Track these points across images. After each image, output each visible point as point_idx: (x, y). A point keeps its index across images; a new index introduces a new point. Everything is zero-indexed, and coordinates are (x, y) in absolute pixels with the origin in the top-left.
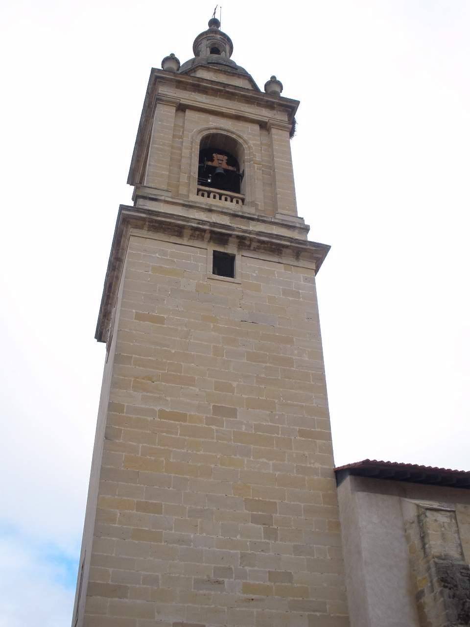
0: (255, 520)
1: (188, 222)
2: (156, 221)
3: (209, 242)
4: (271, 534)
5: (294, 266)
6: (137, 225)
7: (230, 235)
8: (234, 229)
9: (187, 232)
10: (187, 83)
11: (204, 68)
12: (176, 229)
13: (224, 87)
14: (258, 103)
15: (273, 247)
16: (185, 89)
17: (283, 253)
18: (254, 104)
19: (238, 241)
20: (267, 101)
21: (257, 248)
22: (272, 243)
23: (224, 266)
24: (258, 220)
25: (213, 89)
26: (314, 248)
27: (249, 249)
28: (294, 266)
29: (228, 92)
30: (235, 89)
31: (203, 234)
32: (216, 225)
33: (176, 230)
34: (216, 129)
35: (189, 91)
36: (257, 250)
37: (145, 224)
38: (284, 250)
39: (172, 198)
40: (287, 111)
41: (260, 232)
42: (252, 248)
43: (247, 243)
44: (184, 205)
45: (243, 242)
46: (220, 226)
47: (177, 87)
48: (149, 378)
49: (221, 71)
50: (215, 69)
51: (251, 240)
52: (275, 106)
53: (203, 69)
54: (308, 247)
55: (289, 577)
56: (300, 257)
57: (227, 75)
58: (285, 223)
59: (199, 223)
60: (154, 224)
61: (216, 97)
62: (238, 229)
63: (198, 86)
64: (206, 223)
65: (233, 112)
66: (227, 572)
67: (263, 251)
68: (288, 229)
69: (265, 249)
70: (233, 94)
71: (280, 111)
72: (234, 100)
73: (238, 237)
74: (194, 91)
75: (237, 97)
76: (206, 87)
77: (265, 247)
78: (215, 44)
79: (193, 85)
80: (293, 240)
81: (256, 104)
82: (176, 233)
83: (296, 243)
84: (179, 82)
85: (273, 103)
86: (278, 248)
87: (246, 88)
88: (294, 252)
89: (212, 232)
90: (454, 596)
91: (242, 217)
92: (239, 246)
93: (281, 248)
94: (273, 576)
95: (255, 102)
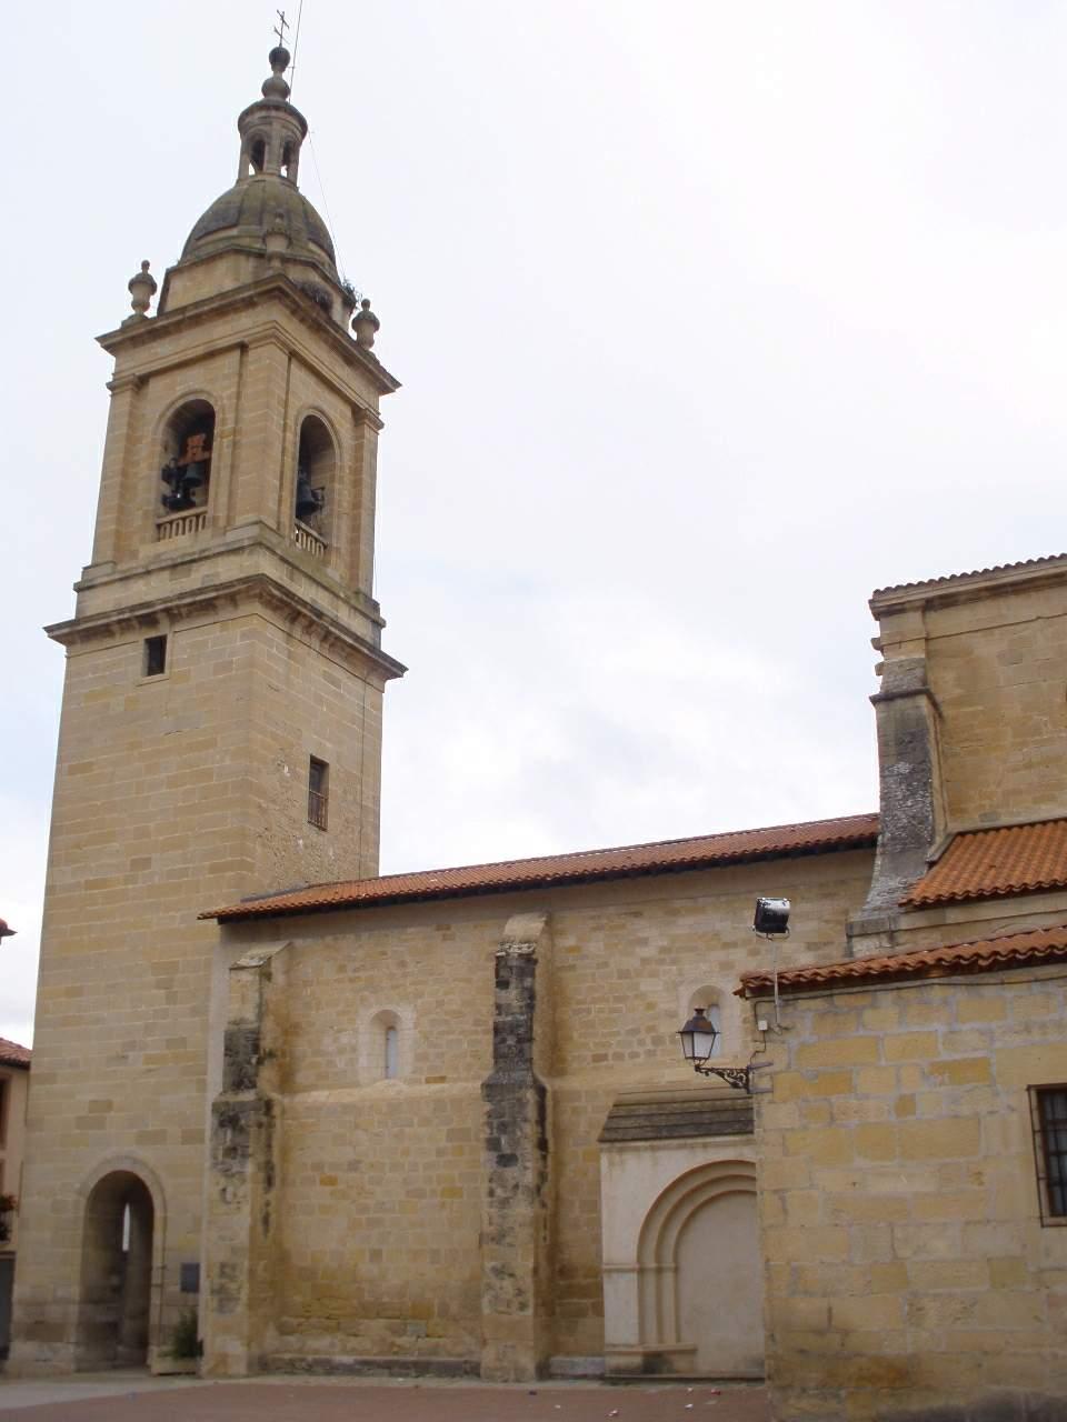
0: (159, 986)
3: (141, 628)
4: (171, 998)
10: (141, 335)
12: (103, 629)
16: (144, 343)
20: (243, 300)
23: (156, 656)
24: (200, 559)
29: (190, 318)
39: (108, 575)
40: (275, 297)
43: (176, 612)
44: (121, 579)
45: (173, 614)
48: (78, 846)
51: (178, 607)
55: (183, 1041)
63: (156, 330)
65: (200, 351)
66: (132, 1045)
69: (197, 610)
78: (253, 137)
83: (224, 588)
90: (232, 1064)
91: (183, 564)
94: (170, 1043)
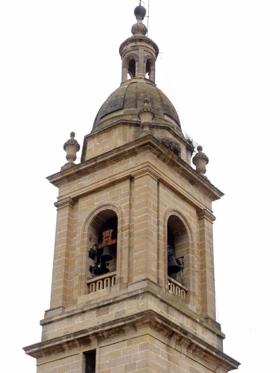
1: (61, 340)
2: (46, 348)
5: (134, 338)
6: (38, 356)
7: (88, 336)
8: (88, 331)
9: (65, 346)
11: (90, 138)
13: (96, 161)
14: (124, 157)
15: (117, 329)
16: (74, 179)
17: (125, 330)
18: (122, 159)
19: (95, 336)
20: (129, 151)
21: (108, 335)
22: (115, 328)
25: (90, 167)
26: (141, 317)
27: (105, 339)
28: (134, 338)
29: (100, 163)
30: (103, 157)
31: (74, 343)
32: (76, 333)
33: (59, 348)
34: (98, 208)
35: (78, 179)
36: (110, 337)
37: (41, 353)
38: (124, 328)
40: (147, 148)
41: (103, 324)
42: (106, 337)
43: (100, 335)
46: (78, 333)
47: (69, 181)
49: (101, 132)
50: (96, 133)
51: (102, 332)
52: (136, 151)
53: (90, 139)
54: (136, 319)
56: (138, 328)
57: (107, 132)
58: (131, 295)
59: (67, 338)
60: (46, 351)
61: (95, 171)
62: (90, 329)
63: (80, 171)
64: (71, 335)
65: (107, 182)
67: (113, 335)
68: (135, 299)
69: (113, 333)
70: (104, 162)
71: (142, 151)
72: (108, 166)
73: (93, 334)
74: (80, 177)
75: (108, 162)
76: (85, 169)
77: (112, 332)
79: (77, 173)
80: (125, 319)
81: (123, 158)
82: (61, 350)
84: (68, 177)
85: (134, 149)
86: (119, 329)
87: (109, 151)
88: (130, 326)
89: (78, 339)
92: (98, 339)
93: (122, 328)
95: (122, 157)
